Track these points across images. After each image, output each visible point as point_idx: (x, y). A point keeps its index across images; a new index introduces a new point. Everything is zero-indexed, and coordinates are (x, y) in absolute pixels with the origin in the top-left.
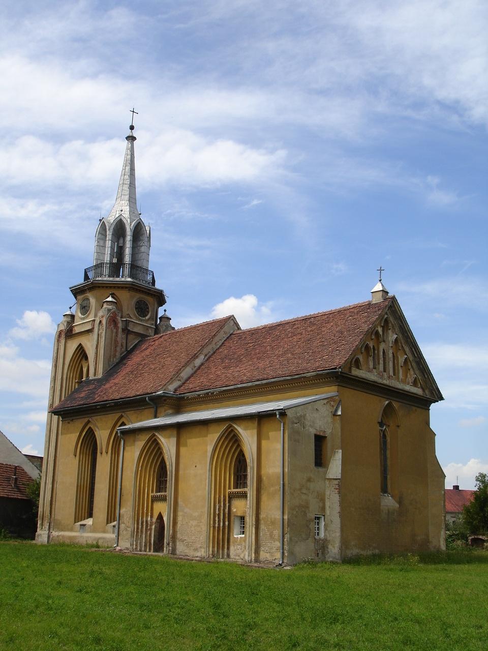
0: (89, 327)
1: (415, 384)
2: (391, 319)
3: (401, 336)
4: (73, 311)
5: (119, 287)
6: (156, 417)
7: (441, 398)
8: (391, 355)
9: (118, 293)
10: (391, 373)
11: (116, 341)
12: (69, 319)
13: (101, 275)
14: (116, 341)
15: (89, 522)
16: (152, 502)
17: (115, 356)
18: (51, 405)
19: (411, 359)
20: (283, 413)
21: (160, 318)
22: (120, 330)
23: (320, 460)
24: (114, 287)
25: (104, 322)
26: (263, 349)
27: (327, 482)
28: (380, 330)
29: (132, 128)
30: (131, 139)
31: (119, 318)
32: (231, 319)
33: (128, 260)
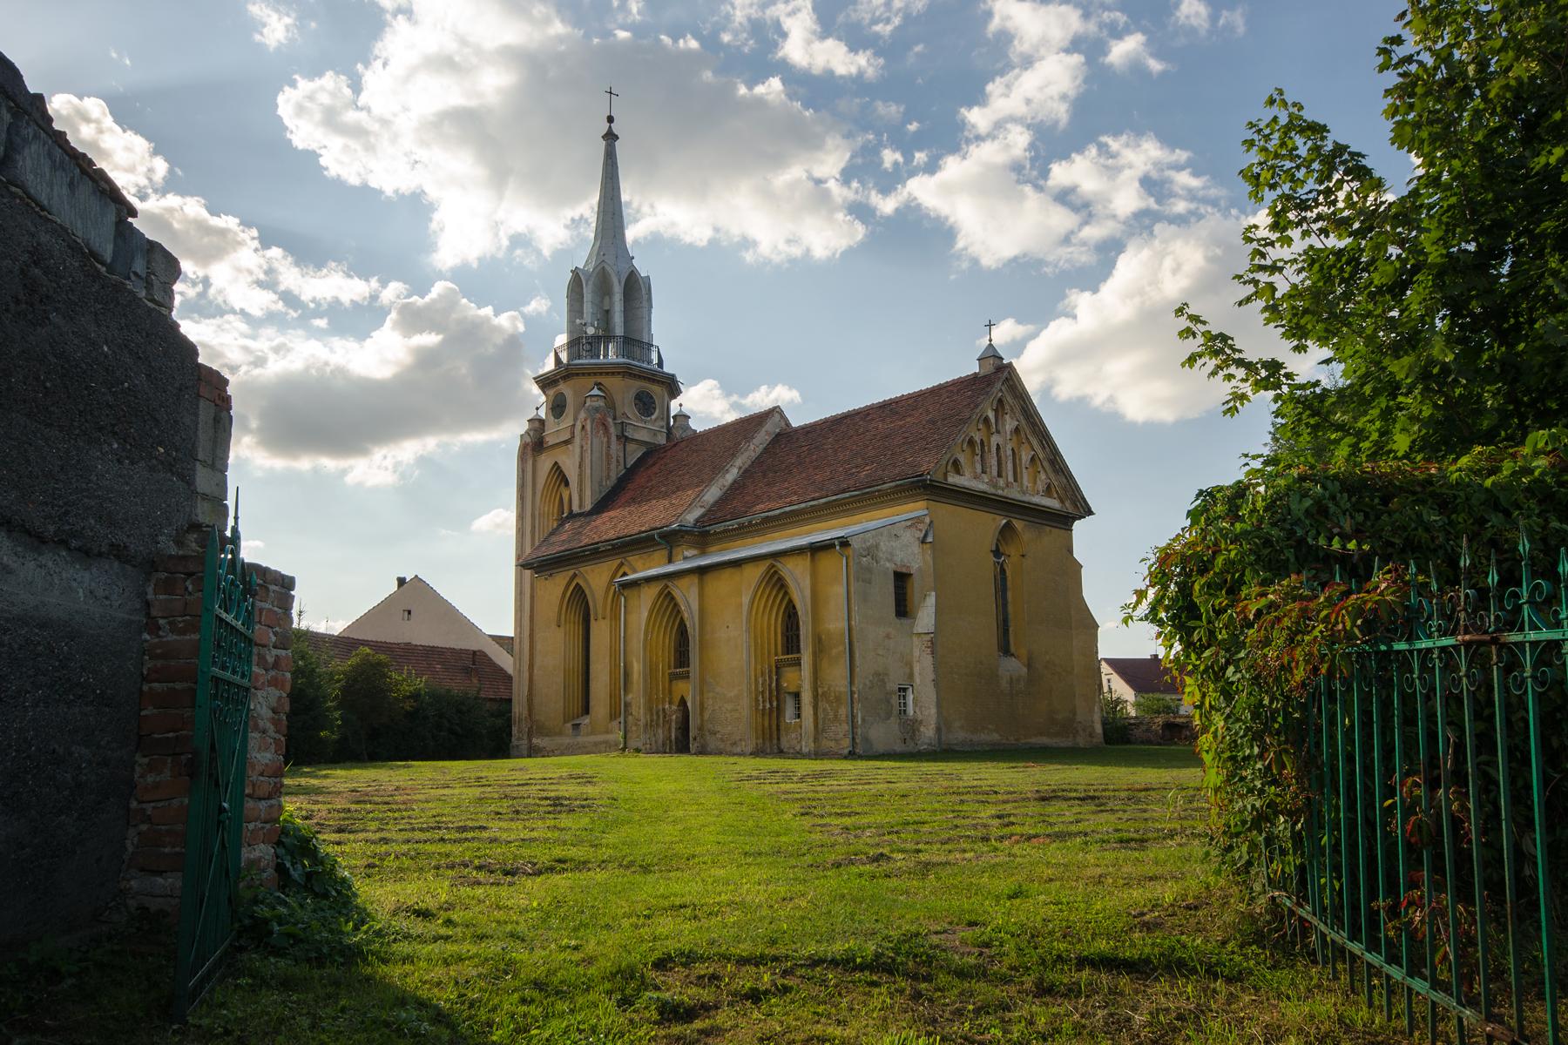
0: (567, 436)
1: (1048, 491)
2: (1009, 399)
3: (1023, 422)
4: (542, 414)
5: (607, 373)
6: (670, 561)
7: (1090, 513)
8: (1009, 452)
9: (606, 381)
10: (1011, 479)
11: (608, 455)
12: (537, 424)
13: (579, 357)
14: (608, 455)
15: (586, 720)
16: (671, 681)
17: (608, 477)
18: (518, 558)
19: (1041, 456)
20: (844, 543)
21: (674, 417)
22: (614, 438)
23: (903, 609)
24: (601, 374)
25: (588, 427)
26: (822, 454)
27: (915, 639)
28: (991, 415)
29: (610, 119)
30: (610, 137)
31: (610, 420)
32: (775, 411)
33: (893, 108)
